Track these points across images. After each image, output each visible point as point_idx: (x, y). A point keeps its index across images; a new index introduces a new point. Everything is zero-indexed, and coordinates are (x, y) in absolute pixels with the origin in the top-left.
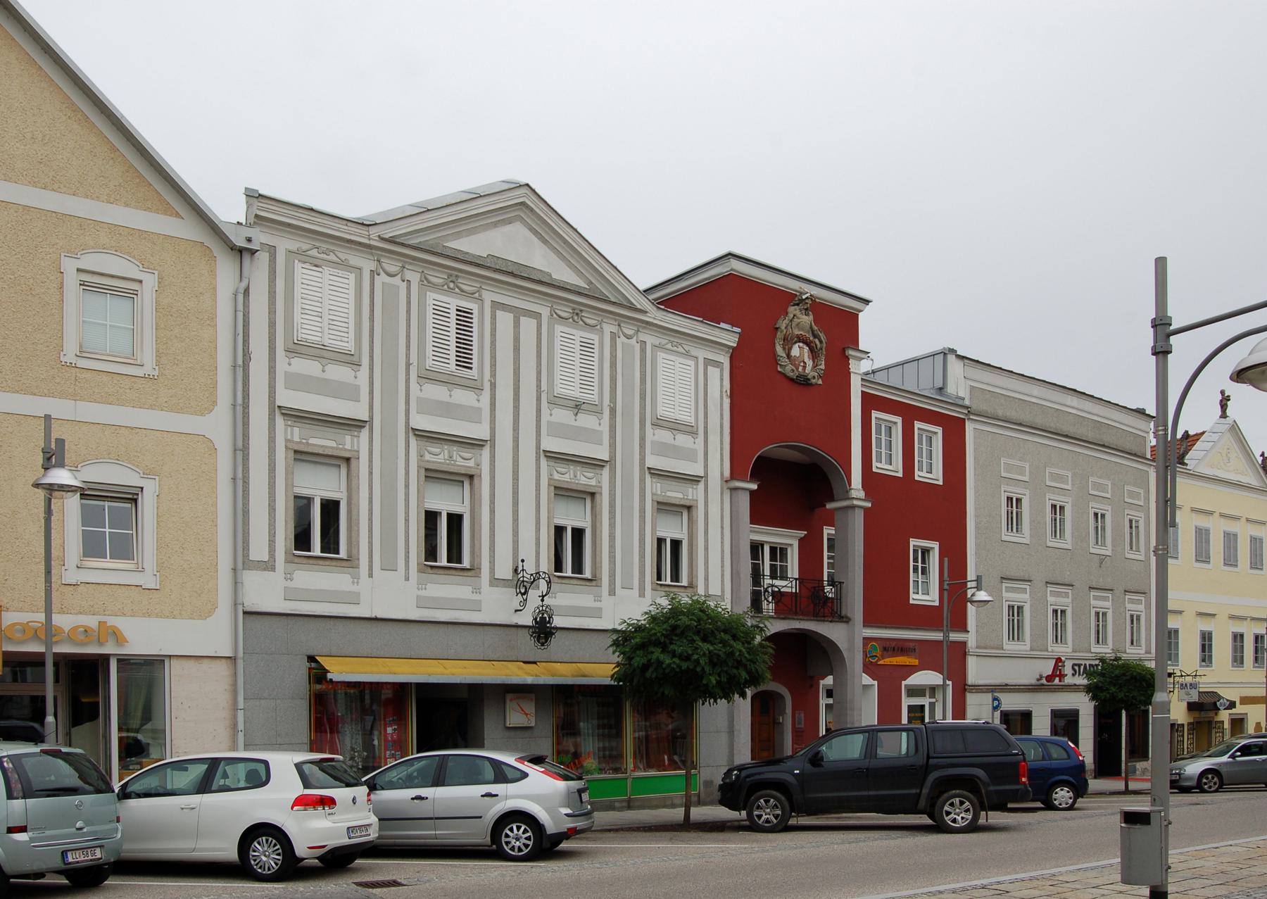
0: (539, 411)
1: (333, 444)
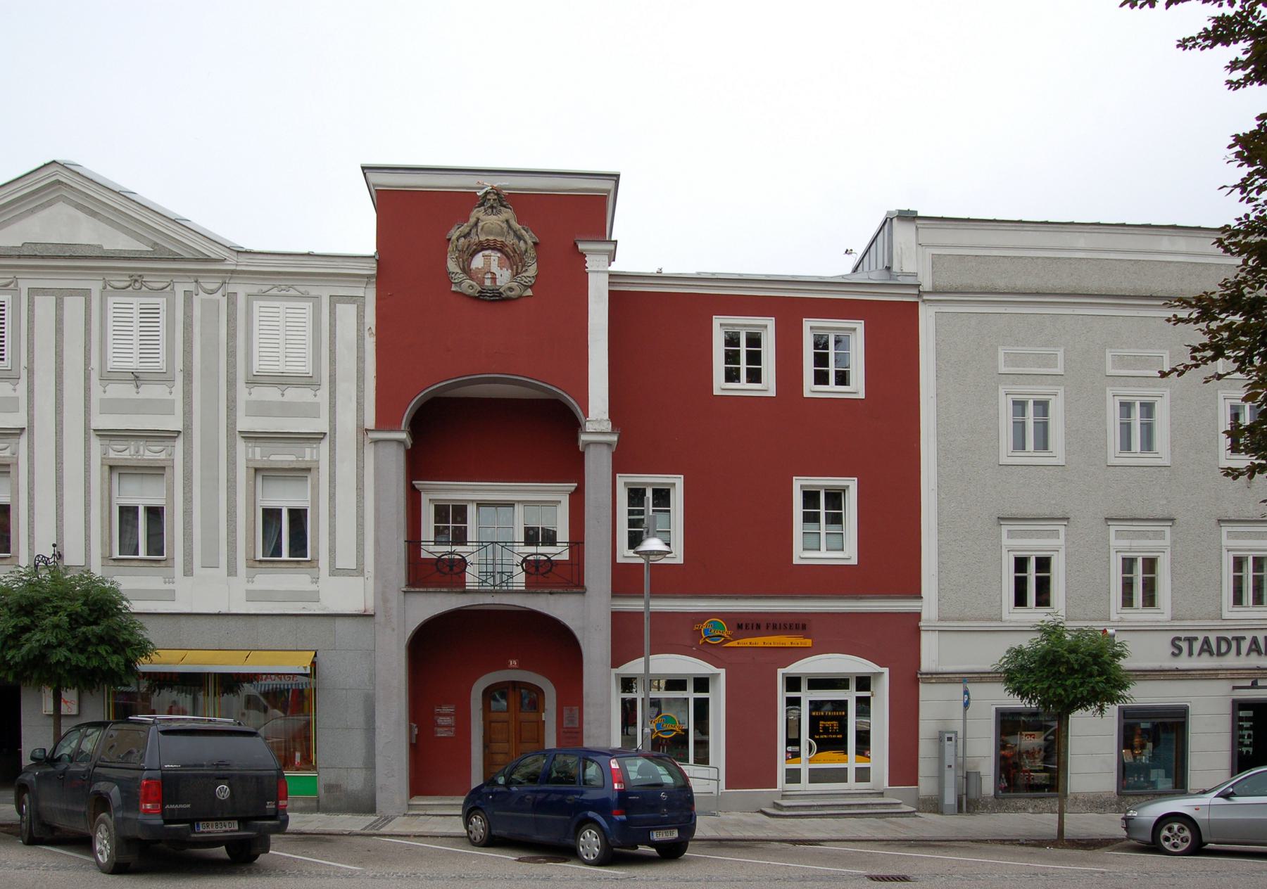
0: (87, 390)
1: (293, 458)
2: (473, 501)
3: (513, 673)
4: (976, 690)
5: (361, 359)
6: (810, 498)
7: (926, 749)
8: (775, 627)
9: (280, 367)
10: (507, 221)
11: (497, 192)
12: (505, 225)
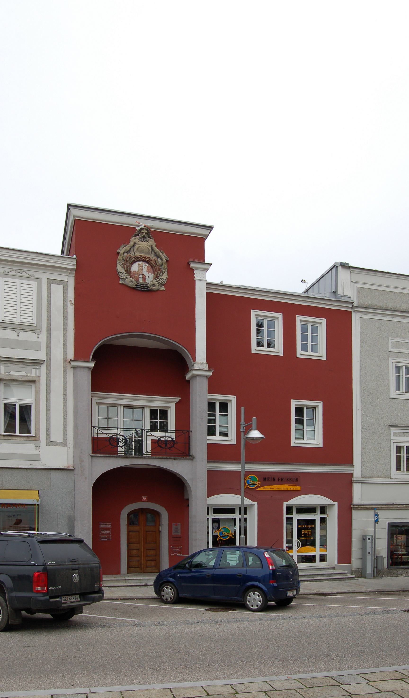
1: (24, 374)
2: (121, 405)
3: (144, 504)
4: (381, 513)
5: (65, 318)
6: (299, 411)
7: (356, 544)
8: (282, 479)
9: (18, 319)
10: (151, 246)
11: (148, 229)
12: (150, 248)
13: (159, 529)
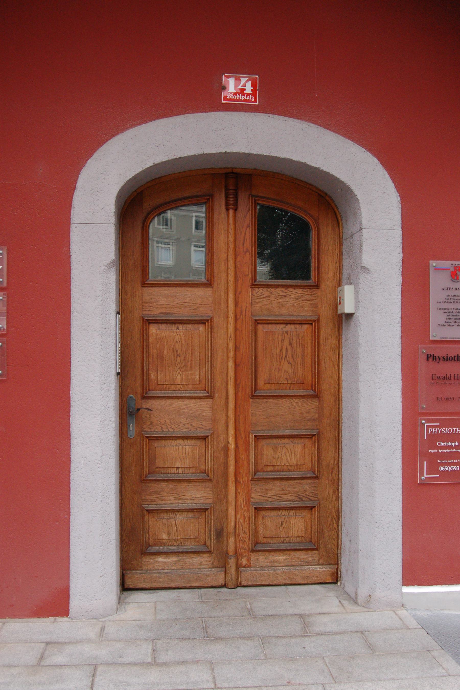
13: (336, 302)
